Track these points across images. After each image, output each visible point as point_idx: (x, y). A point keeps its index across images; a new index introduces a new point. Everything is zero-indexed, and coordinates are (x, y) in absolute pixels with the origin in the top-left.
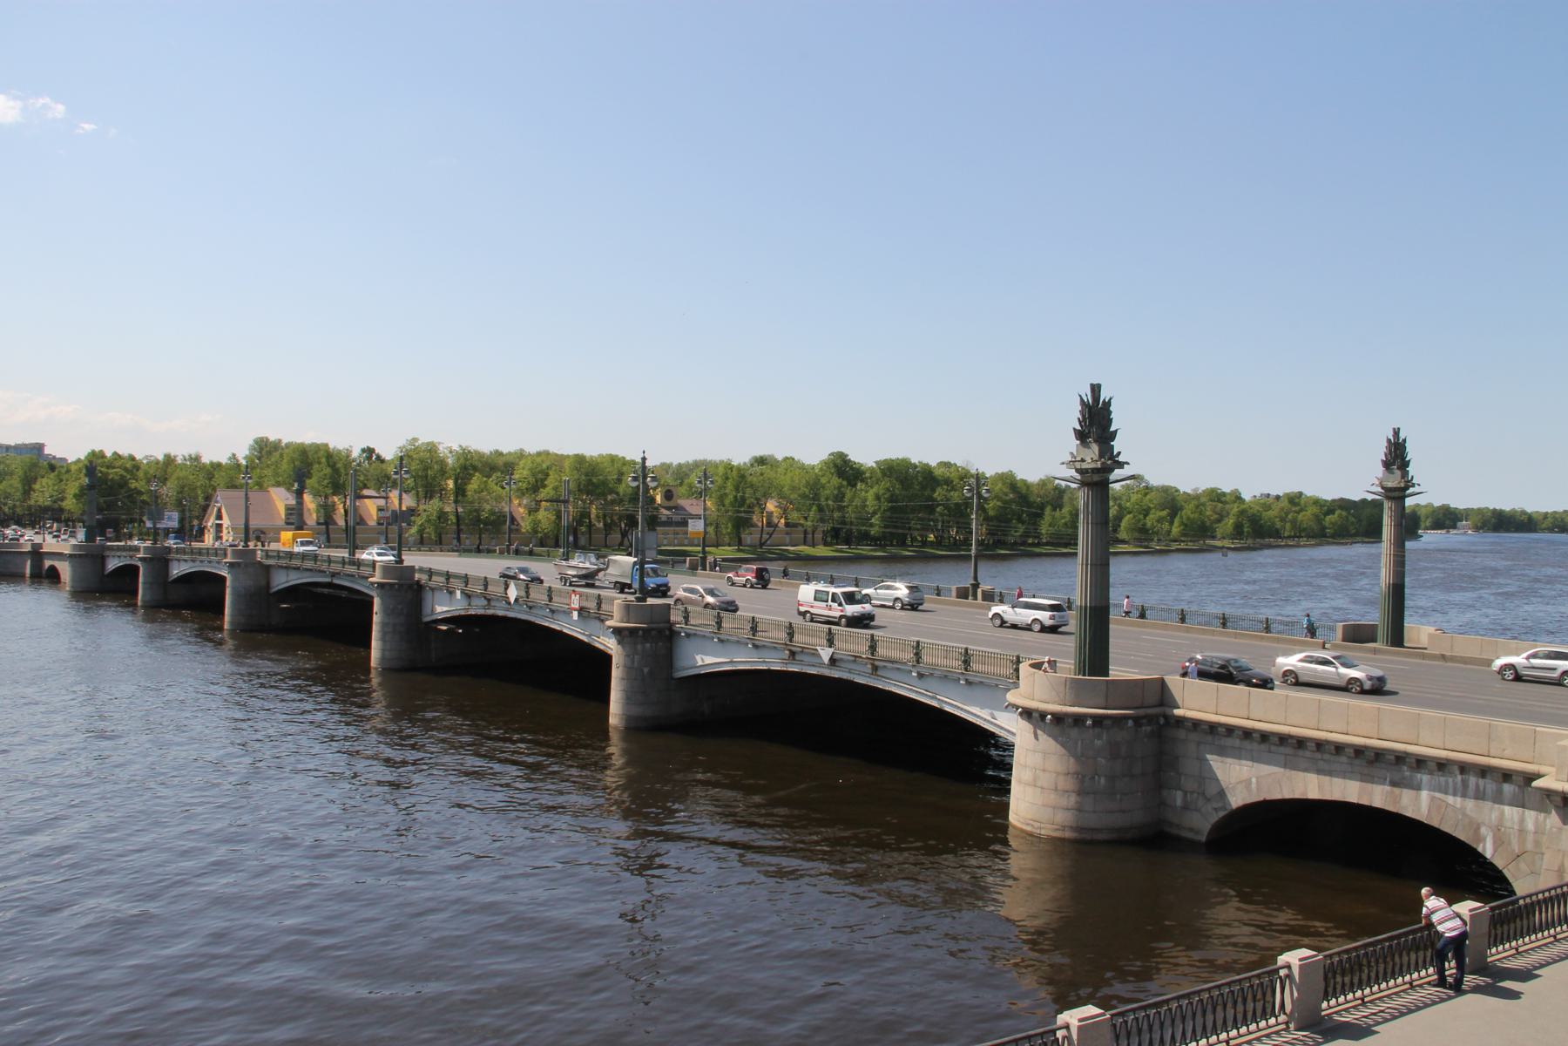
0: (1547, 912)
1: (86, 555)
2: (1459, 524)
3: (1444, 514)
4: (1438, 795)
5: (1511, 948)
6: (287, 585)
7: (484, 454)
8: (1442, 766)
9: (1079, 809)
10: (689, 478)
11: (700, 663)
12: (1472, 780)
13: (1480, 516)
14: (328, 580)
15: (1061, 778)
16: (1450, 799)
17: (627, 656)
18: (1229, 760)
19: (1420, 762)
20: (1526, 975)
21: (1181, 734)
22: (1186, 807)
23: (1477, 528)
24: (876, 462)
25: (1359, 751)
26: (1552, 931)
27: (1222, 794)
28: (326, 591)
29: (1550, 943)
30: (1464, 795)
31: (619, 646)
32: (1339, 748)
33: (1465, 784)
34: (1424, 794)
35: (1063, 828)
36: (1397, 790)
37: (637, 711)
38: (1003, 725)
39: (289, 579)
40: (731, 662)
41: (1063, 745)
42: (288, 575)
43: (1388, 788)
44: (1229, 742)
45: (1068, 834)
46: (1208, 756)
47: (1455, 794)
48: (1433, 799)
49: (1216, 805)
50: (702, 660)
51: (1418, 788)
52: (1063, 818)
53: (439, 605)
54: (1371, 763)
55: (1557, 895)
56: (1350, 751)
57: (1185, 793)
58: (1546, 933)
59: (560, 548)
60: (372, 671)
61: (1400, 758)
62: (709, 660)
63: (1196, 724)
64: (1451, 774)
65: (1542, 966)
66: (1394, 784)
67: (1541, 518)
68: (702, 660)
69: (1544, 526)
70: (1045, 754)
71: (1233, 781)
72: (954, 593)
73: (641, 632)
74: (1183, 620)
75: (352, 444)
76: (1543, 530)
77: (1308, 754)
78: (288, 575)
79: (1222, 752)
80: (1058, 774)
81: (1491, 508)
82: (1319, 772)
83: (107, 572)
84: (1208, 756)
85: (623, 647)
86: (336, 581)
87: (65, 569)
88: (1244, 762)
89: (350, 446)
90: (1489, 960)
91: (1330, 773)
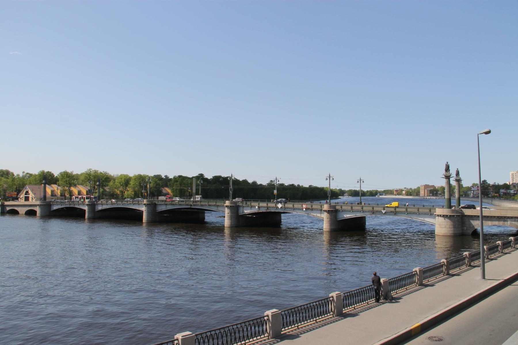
0: (401, 282)
1: (46, 205)
2: (344, 194)
3: (340, 192)
4: (511, 222)
5: (405, 289)
6: (166, 209)
7: (68, 173)
8: (512, 218)
9: (454, 231)
10: (59, 182)
11: (345, 217)
12: (516, 219)
13: (350, 192)
14: (190, 207)
15: (451, 226)
16: (513, 222)
17: (330, 216)
18: (474, 221)
19: (508, 218)
20: (400, 298)
21: (466, 218)
22: (467, 230)
23: (349, 195)
24: (213, 177)
25: (498, 217)
26: (406, 287)
27: (473, 227)
28: (189, 210)
29: (415, 287)
30: (515, 221)
31: (328, 214)
32: (495, 217)
33: (515, 220)
34: (509, 222)
35: (451, 234)
36: (504, 222)
37: (333, 227)
38: (427, 220)
39: (167, 207)
40: (356, 215)
41: (450, 220)
42: (166, 207)
43: (502, 222)
44: (474, 218)
45: (452, 235)
46: (471, 221)
47: (513, 221)
48: (510, 223)
49: (473, 228)
50: (346, 216)
51: (508, 221)
52: (451, 232)
53: (245, 210)
54: (500, 219)
55: (415, 274)
56: (496, 217)
57: (467, 227)
58: (404, 288)
59: (227, 198)
60: (225, 229)
61: (505, 217)
62: (348, 216)
63: (469, 216)
64: (513, 219)
65: (403, 296)
66: (504, 221)
67: (366, 192)
68: (346, 216)
69: (367, 194)
70: (447, 222)
71: (476, 224)
72: (357, 204)
73: (334, 211)
74: (424, 207)
75: (22, 172)
76: (367, 196)
77: (489, 218)
78: (166, 207)
79: (473, 220)
80: (450, 225)
81: (353, 190)
82: (491, 221)
83: (52, 210)
84: (471, 221)
85: (329, 214)
86: (192, 207)
87: (38, 209)
88: (477, 221)
89: (73, 171)
90: (423, 283)
91: (493, 221)
